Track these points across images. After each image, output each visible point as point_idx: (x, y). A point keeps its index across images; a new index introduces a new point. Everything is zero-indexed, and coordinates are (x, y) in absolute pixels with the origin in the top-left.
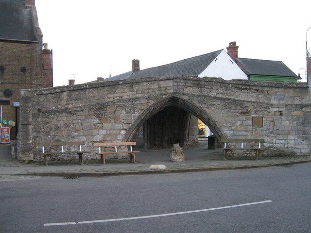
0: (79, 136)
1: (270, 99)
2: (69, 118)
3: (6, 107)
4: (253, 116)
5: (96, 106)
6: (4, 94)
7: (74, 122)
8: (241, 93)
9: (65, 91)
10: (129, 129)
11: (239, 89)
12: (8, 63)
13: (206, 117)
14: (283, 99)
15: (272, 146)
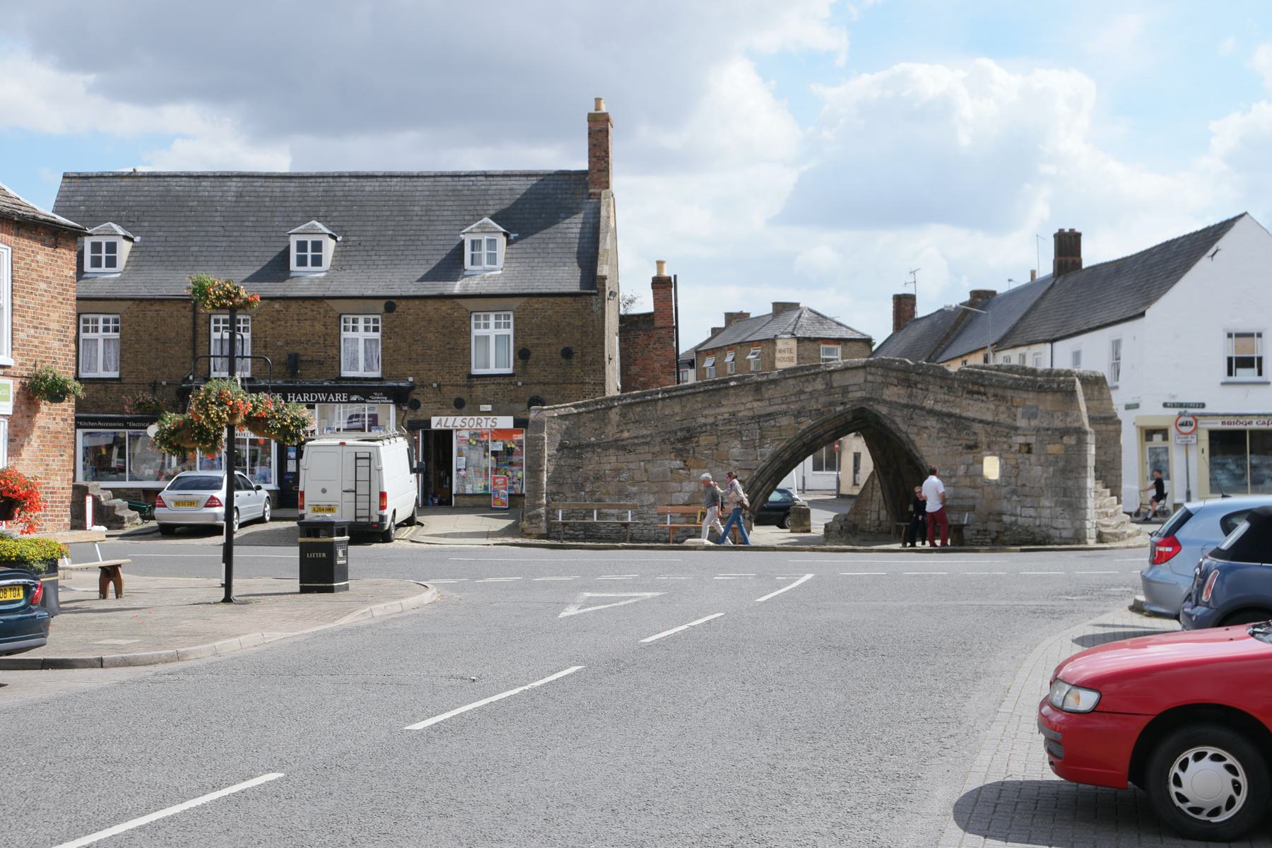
0: (641, 493)
2: (622, 458)
5: (676, 433)
7: (631, 466)
8: (972, 402)
9: (615, 407)
11: (971, 392)
12: (536, 341)
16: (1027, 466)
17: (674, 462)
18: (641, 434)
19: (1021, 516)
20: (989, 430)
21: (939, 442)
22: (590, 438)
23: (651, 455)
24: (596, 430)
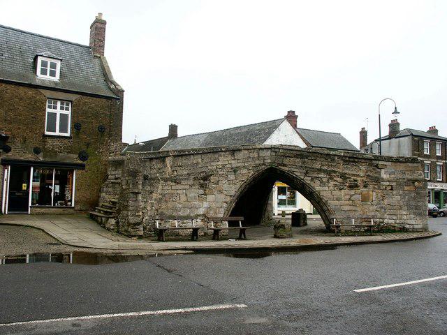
3: (80, 172)
6: (79, 156)
7: (179, 192)
15: (383, 223)
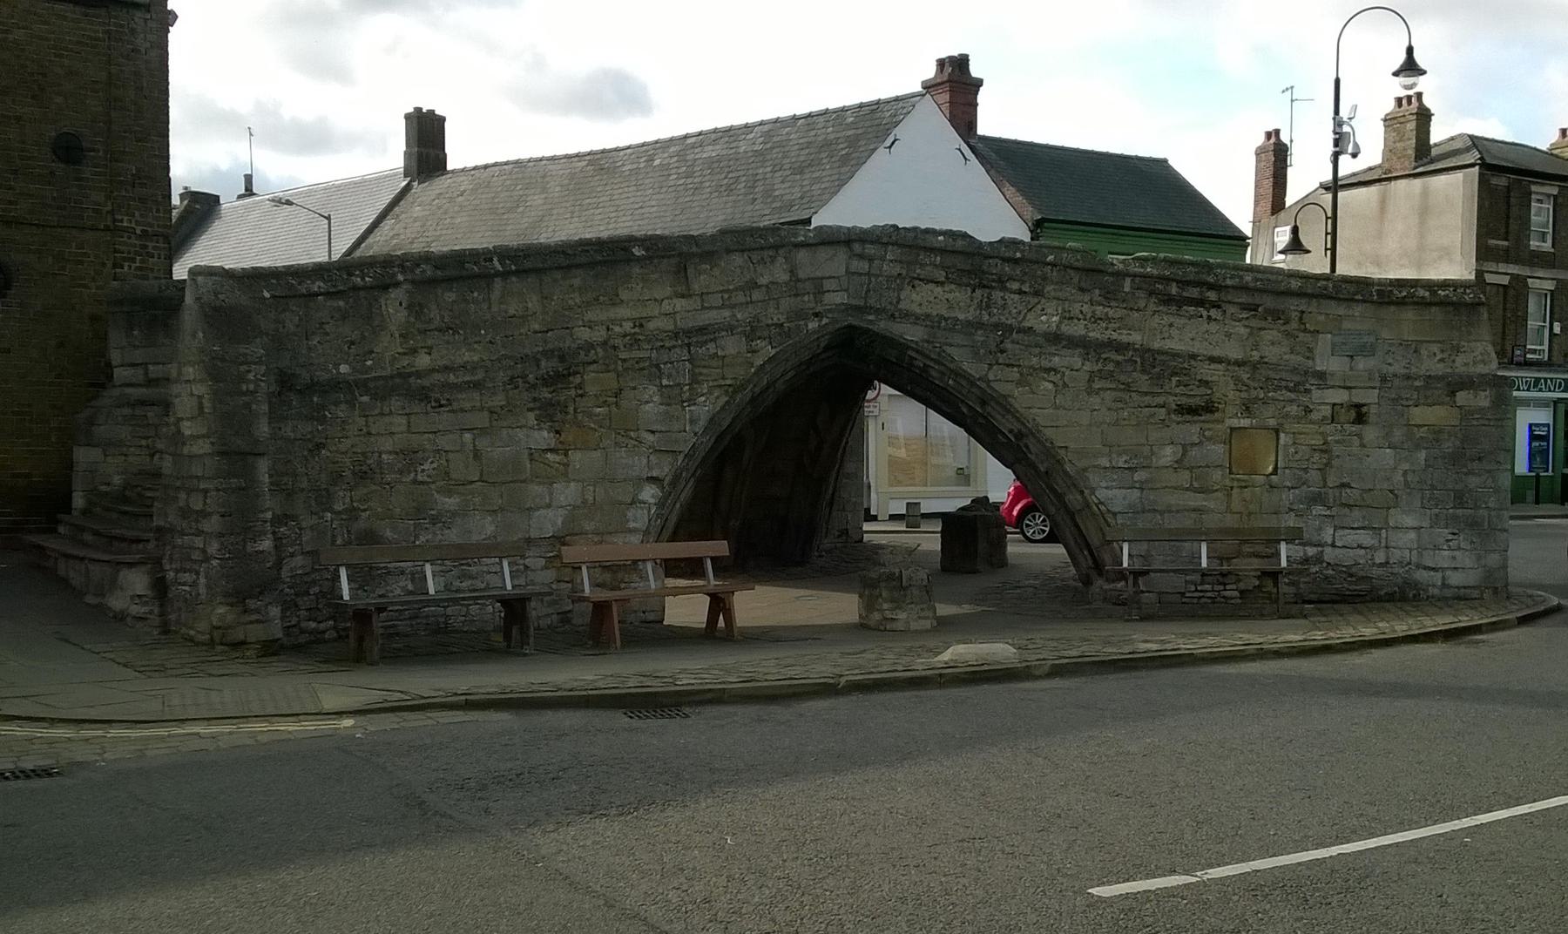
1: (1310, 350)
4: (1235, 423)
5: (537, 362)
7: (443, 442)
8: (1179, 322)
9: (397, 284)
10: (676, 479)
11: (1168, 300)
13: (1005, 424)
14: (1367, 350)
15: (1319, 559)
16: (1355, 449)
17: (536, 434)
18: (459, 361)
19: (1333, 545)
20: (1245, 376)
21: (1095, 401)
22: (337, 366)
23: (486, 414)
24: (352, 343)
